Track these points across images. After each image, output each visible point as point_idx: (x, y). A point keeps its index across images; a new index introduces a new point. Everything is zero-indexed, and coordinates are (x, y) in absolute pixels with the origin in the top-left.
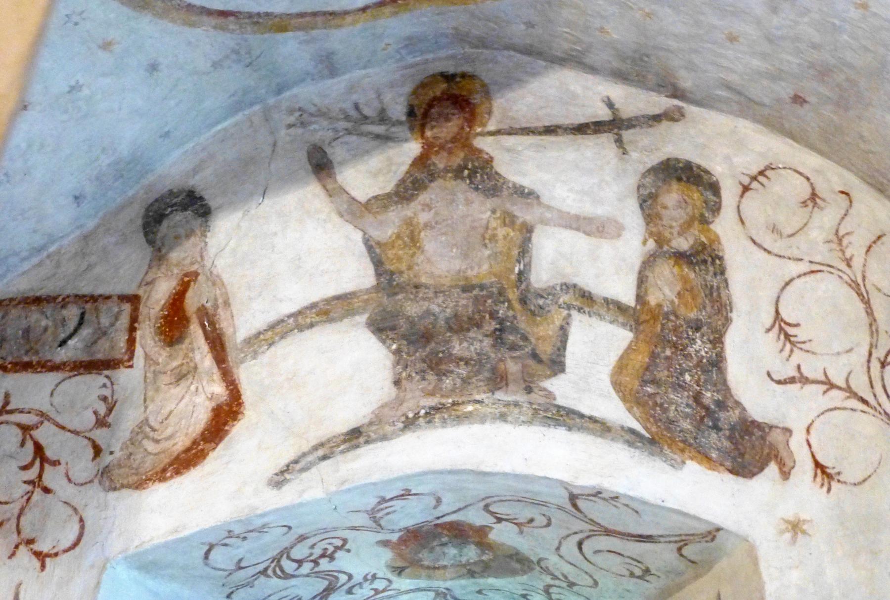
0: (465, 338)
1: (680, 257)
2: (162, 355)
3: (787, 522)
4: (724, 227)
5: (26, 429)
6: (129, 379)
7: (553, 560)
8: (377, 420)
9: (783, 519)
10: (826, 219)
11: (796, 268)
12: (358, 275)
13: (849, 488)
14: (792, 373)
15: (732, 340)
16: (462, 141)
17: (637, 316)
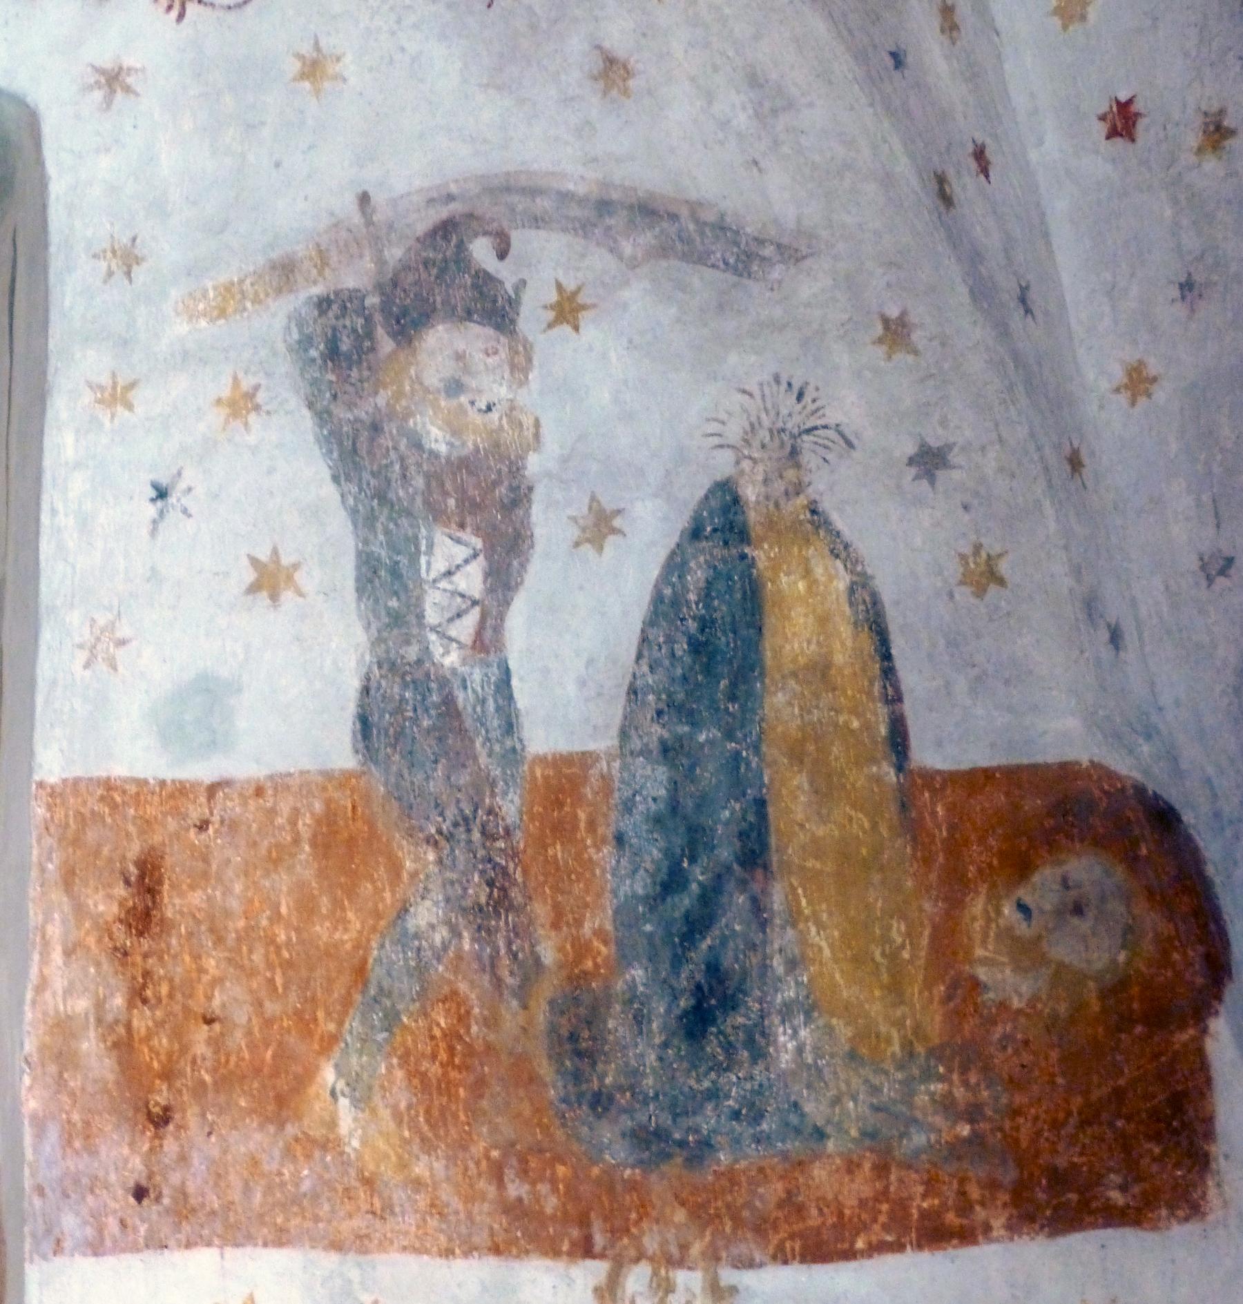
3: (102, 72)
9: (93, 66)
13: (221, 13)
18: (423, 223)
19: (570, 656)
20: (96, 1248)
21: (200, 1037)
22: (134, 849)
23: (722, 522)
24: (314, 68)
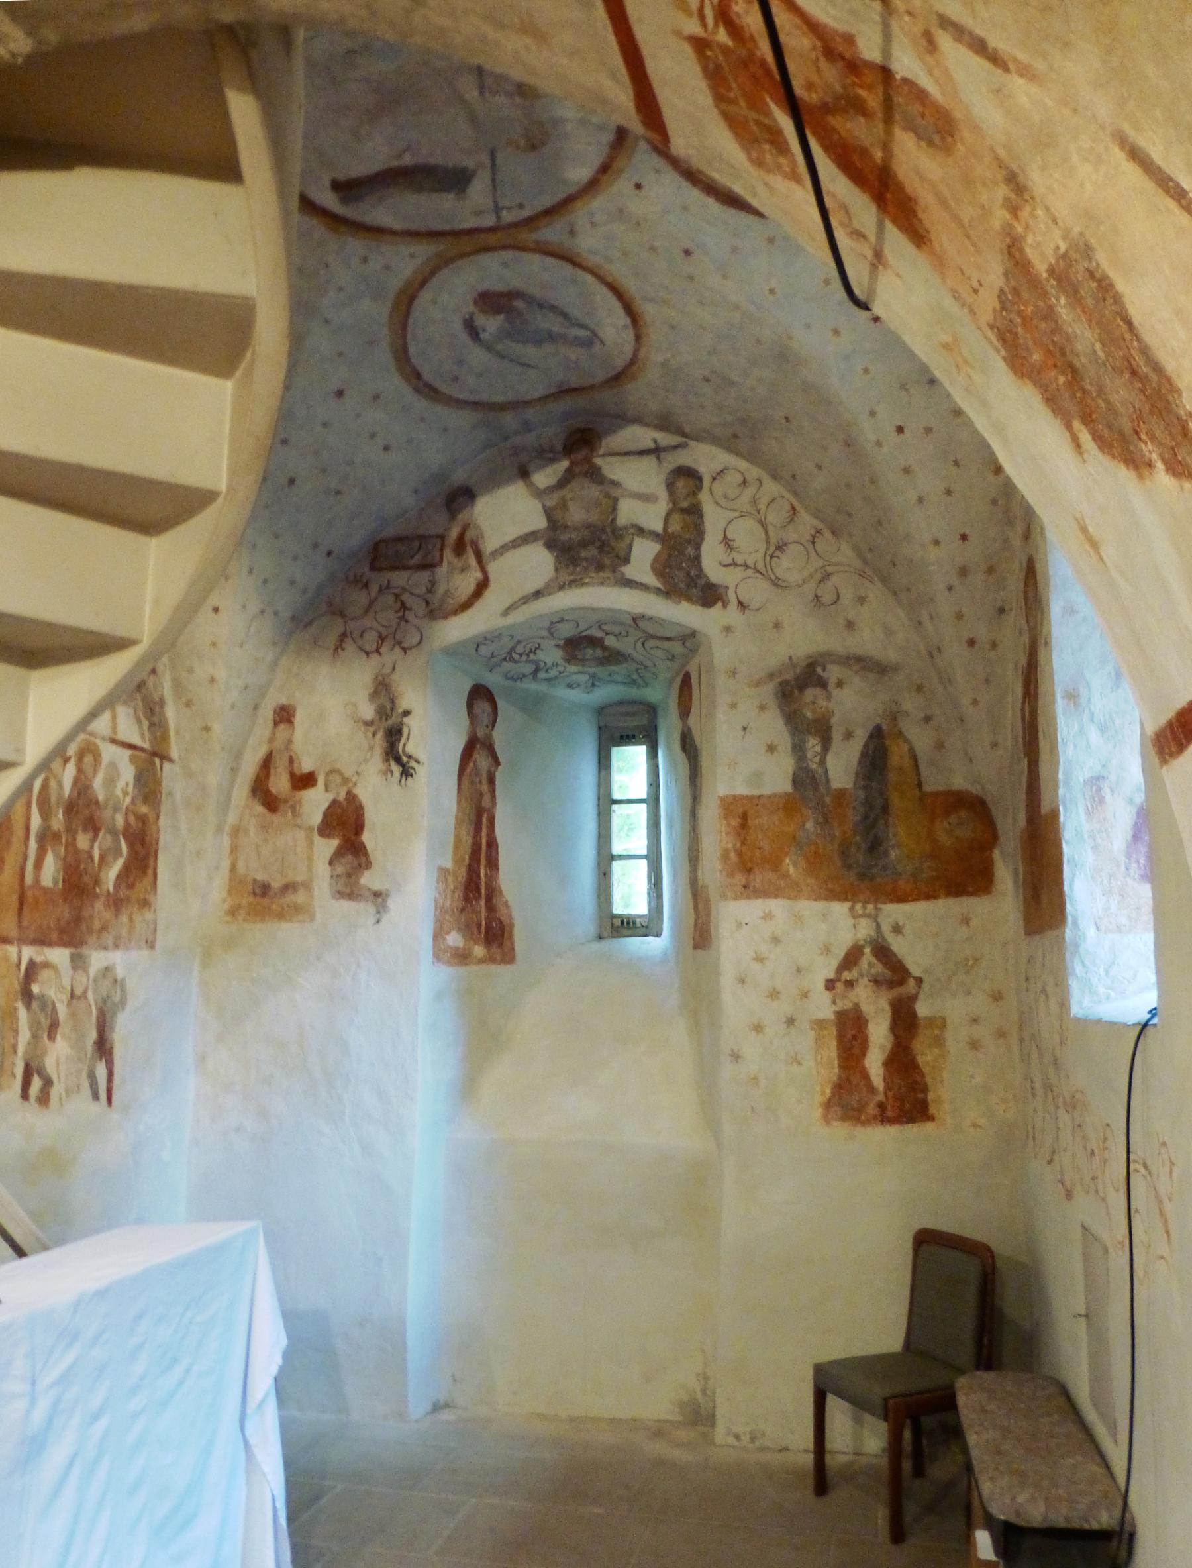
0: (587, 548)
1: (683, 511)
2: (455, 561)
4: (704, 496)
5: (397, 596)
6: (442, 571)
7: (635, 654)
8: (547, 586)
10: (749, 492)
11: (733, 515)
12: (539, 522)
14: (730, 561)
15: (705, 548)
16: (588, 460)
17: (663, 538)
18: (804, 664)
19: (841, 767)
20: (735, 899)
21: (757, 853)
22: (741, 811)
23: (877, 735)
24: (777, 626)
